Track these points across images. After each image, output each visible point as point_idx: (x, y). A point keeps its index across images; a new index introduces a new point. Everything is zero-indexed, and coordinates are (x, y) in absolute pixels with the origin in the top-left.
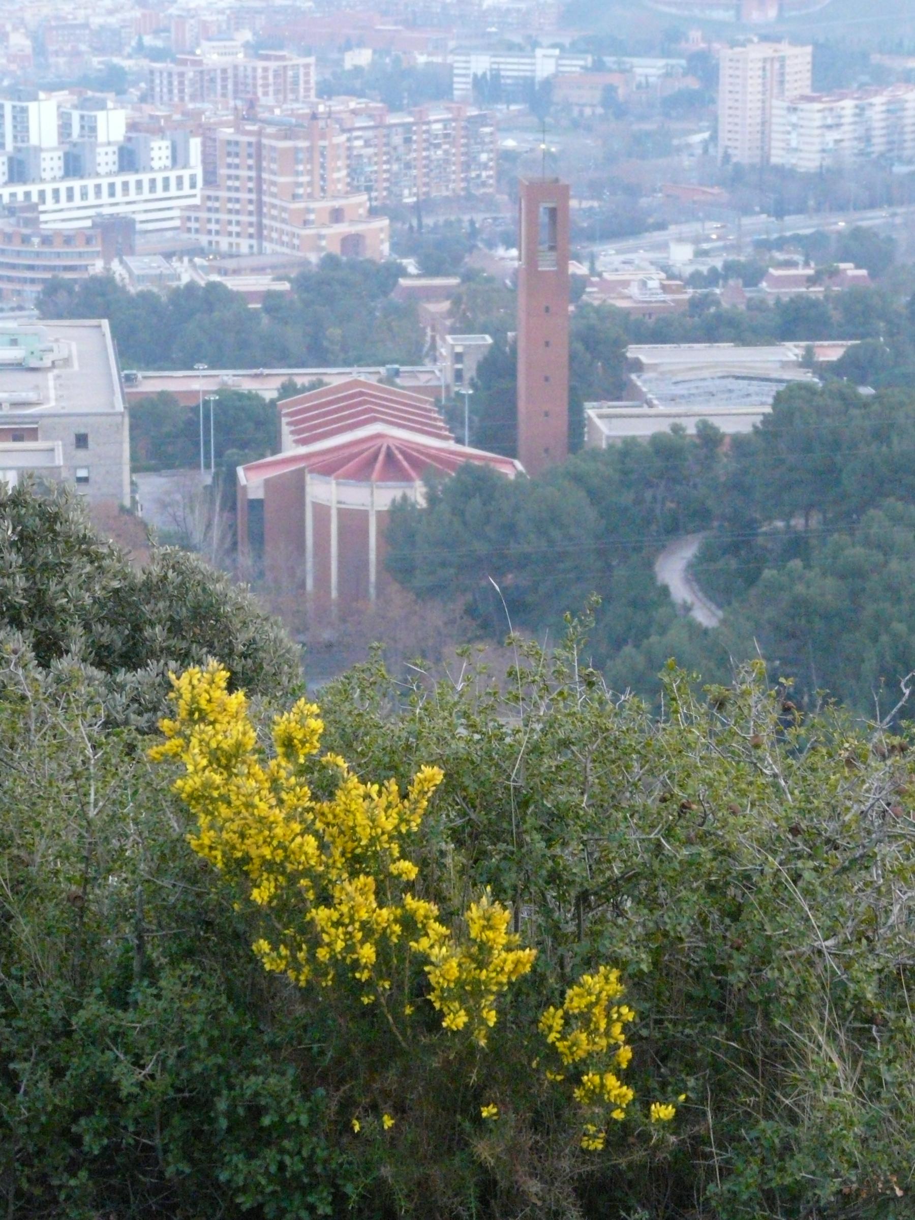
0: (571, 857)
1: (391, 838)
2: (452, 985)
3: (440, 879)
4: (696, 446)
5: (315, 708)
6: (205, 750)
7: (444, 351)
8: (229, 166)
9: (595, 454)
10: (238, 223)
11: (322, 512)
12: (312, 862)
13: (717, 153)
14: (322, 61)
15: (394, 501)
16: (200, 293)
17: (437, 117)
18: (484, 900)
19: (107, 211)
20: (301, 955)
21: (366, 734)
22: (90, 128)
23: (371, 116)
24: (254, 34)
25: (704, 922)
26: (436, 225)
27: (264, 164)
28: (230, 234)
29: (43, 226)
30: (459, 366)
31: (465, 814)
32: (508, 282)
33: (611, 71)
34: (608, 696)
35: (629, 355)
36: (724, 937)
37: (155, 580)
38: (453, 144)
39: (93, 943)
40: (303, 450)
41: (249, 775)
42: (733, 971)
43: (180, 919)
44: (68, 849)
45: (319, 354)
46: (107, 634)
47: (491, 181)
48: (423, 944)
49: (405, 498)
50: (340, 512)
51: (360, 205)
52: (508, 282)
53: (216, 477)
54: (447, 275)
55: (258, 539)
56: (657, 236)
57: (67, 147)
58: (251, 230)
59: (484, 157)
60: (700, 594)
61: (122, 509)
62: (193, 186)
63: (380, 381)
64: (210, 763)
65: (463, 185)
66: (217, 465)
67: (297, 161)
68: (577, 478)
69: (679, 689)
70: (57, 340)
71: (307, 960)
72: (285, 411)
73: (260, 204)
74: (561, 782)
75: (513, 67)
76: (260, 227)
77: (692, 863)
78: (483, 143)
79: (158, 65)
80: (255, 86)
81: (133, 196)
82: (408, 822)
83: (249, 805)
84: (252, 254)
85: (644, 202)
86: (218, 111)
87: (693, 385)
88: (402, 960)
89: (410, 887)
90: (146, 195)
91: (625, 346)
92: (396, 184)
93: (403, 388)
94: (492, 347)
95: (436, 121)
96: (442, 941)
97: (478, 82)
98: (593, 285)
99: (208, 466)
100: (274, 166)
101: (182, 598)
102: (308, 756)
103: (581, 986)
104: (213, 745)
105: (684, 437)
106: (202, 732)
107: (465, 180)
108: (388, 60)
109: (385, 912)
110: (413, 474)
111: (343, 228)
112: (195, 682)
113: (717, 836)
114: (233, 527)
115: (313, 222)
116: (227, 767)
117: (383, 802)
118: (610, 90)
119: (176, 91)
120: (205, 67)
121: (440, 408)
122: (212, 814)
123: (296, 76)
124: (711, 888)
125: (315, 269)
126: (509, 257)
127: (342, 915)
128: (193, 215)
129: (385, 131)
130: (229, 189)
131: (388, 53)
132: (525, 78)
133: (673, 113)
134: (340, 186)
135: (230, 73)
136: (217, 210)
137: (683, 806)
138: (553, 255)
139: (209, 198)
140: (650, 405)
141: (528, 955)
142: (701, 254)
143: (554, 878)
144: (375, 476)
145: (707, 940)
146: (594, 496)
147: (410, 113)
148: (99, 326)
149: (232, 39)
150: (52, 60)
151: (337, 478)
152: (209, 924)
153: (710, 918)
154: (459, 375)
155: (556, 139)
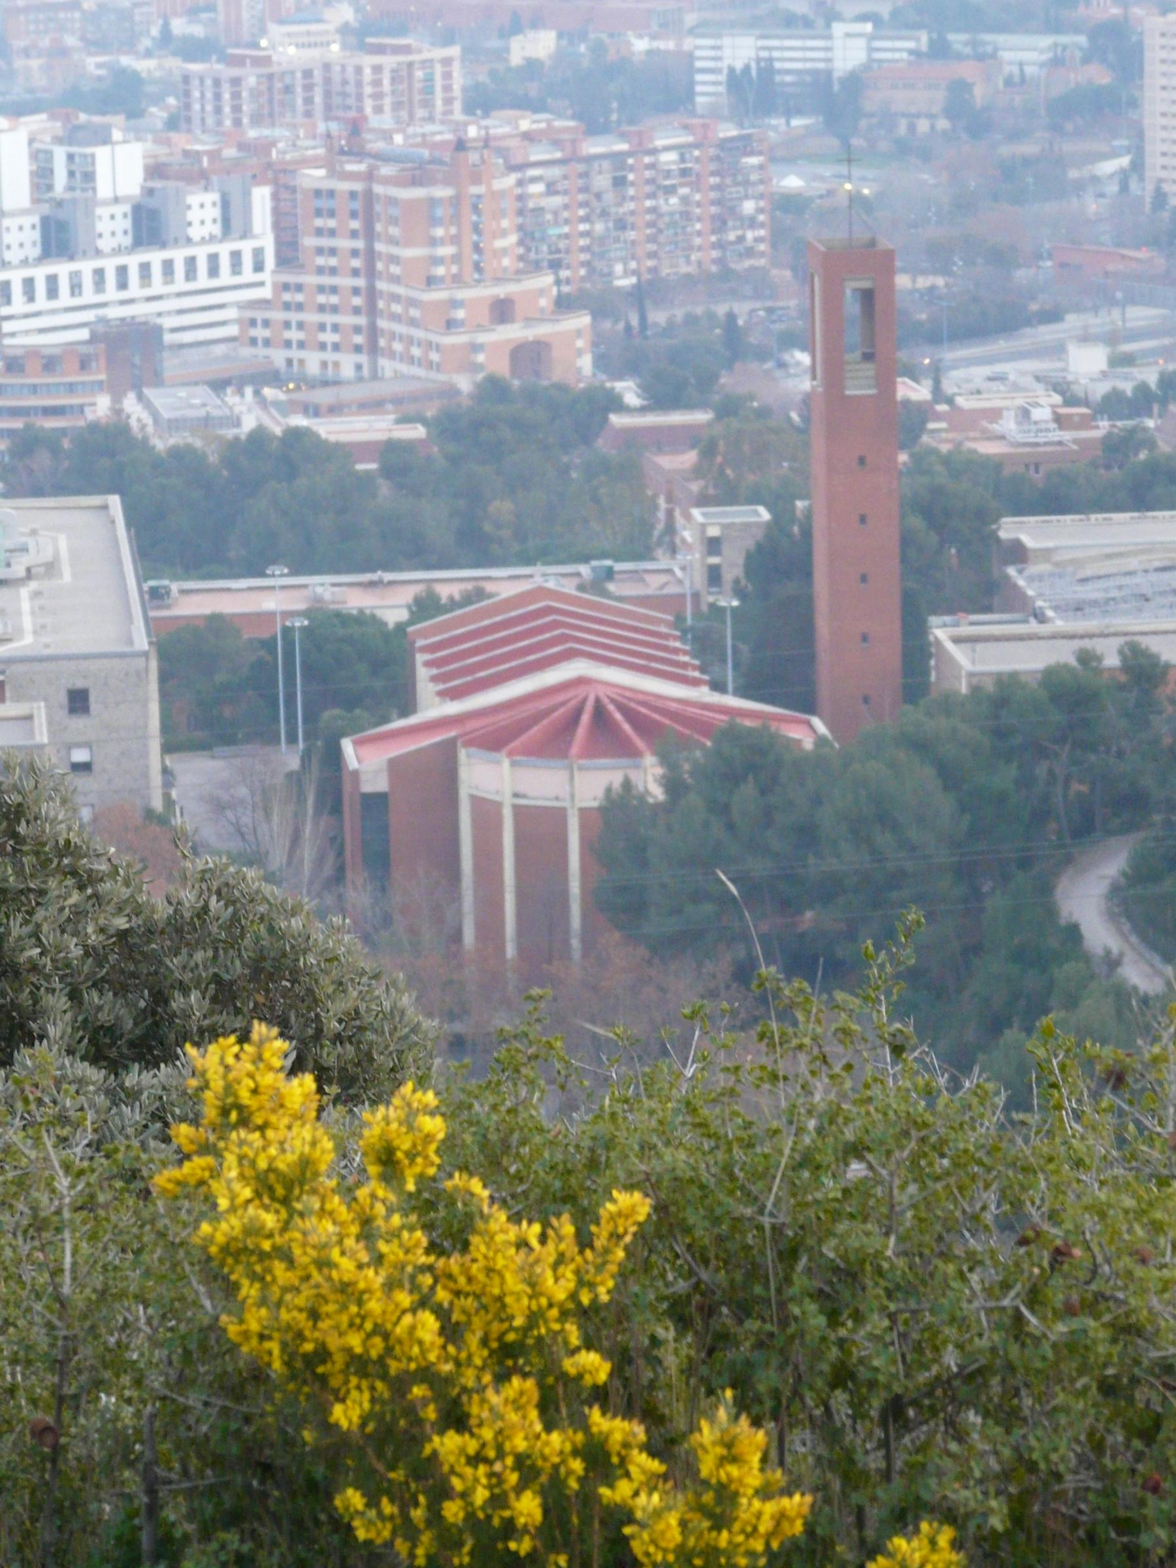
0: (872, 1341)
1: (564, 1315)
2: (671, 1558)
3: (652, 1385)
4: (1122, 688)
5: (430, 1098)
6: (248, 1172)
7: (687, 535)
8: (319, 232)
9: (948, 704)
10: (336, 328)
11: (486, 812)
12: (432, 1357)
13: (1143, 191)
14: (471, 53)
15: (609, 790)
16: (275, 445)
17: (668, 141)
18: (722, 1414)
19: (114, 313)
20: (418, 1514)
21: (523, 1142)
22: (84, 176)
23: (557, 144)
24: (357, 11)
25: (1099, 1448)
26: (671, 324)
27: (379, 227)
28: (323, 346)
29: (7, 341)
30: (714, 560)
31: (691, 1273)
32: (795, 416)
33: (959, 57)
34: (942, 1081)
35: (1003, 535)
36: (1133, 1471)
37: (187, 915)
38: (696, 186)
39: (74, 1506)
40: (453, 708)
41: (323, 1212)
42: (1149, 1528)
43: (218, 1462)
44: (29, 1348)
45: (476, 546)
46: (106, 1006)
47: (762, 247)
48: (622, 1491)
49: (627, 785)
50: (518, 811)
51: (541, 292)
52: (795, 416)
53: (306, 758)
54: (690, 406)
55: (380, 862)
56: (1046, 333)
57: (46, 209)
58: (359, 339)
59: (749, 207)
60: (1134, 939)
61: (149, 814)
62: (259, 267)
63: (581, 588)
64: (258, 1194)
65: (715, 254)
66: (307, 737)
67: (434, 222)
68: (920, 746)
69: (1063, 1067)
70: (34, 532)
71: (429, 1523)
72: (420, 643)
73: (372, 295)
74: (852, 1216)
75: (794, 55)
76: (373, 332)
77: (1074, 1346)
78: (747, 183)
79: (195, 67)
80: (360, 97)
81: (158, 285)
82: (592, 1286)
83: (324, 1264)
84: (360, 379)
85: (1022, 275)
86: (297, 141)
87: (1111, 583)
88: (586, 1521)
89: (600, 1396)
90: (180, 284)
91: (996, 520)
92: (601, 256)
93: (621, 599)
94: (768, 525)
95: (667, 149)
96: (652, 1483)
97: (736, 81)
98: (938, 417)
99: (292, 739)
100: (394, 231)
101: (232, 944)
102: (421, 1178)
103: (890, 1555)
104: (262, 1164)
105: (1098, 671)
106: (242, 1143)
107: (719, 245)
108: (582, 48)
109: (555, 1437)
110: (639, 743)
111: (513, 332)
112: (230, 1060)
113: (1116, 1300)
114: (336, 842)
115: (461, 323)
116: (286, 1201)
117: (550, 1252)
118: (960, 88)
119: (227, 109)
120: (275, 69)
121: (684, 632)
122: (262, 1279)
123: (429, 79)
124: (1108, 1388)
125: (466, 402)
126: (799, 375)
127: (484, 1445)
128: (259, 315)
129: (581, 168)
130: (320, 271)
131: (583, 36)
132: (815, 73)
133: (1069, 127)
134: (506, 262)
135: (318, 75)
136: (300, 307)
137: (1058, 1252)
138: (869, 369)
139: (286, 287)
140: (1041, 618)
141: (797, 1503)
142: (1120, 361)
143: (842, 1376)
144: (575, 749)
145: (1103, 1475)
146: (949, 776)
147: (623, 136)
148: (105, 507)
149: (320, 21)
150: (19, 63)
151: (510, 754)
152: (266, 1469)
153: (1110, 1440)
154: (714, 576)
155: (870, 174)
